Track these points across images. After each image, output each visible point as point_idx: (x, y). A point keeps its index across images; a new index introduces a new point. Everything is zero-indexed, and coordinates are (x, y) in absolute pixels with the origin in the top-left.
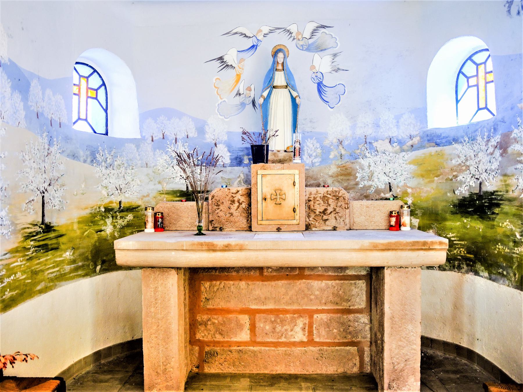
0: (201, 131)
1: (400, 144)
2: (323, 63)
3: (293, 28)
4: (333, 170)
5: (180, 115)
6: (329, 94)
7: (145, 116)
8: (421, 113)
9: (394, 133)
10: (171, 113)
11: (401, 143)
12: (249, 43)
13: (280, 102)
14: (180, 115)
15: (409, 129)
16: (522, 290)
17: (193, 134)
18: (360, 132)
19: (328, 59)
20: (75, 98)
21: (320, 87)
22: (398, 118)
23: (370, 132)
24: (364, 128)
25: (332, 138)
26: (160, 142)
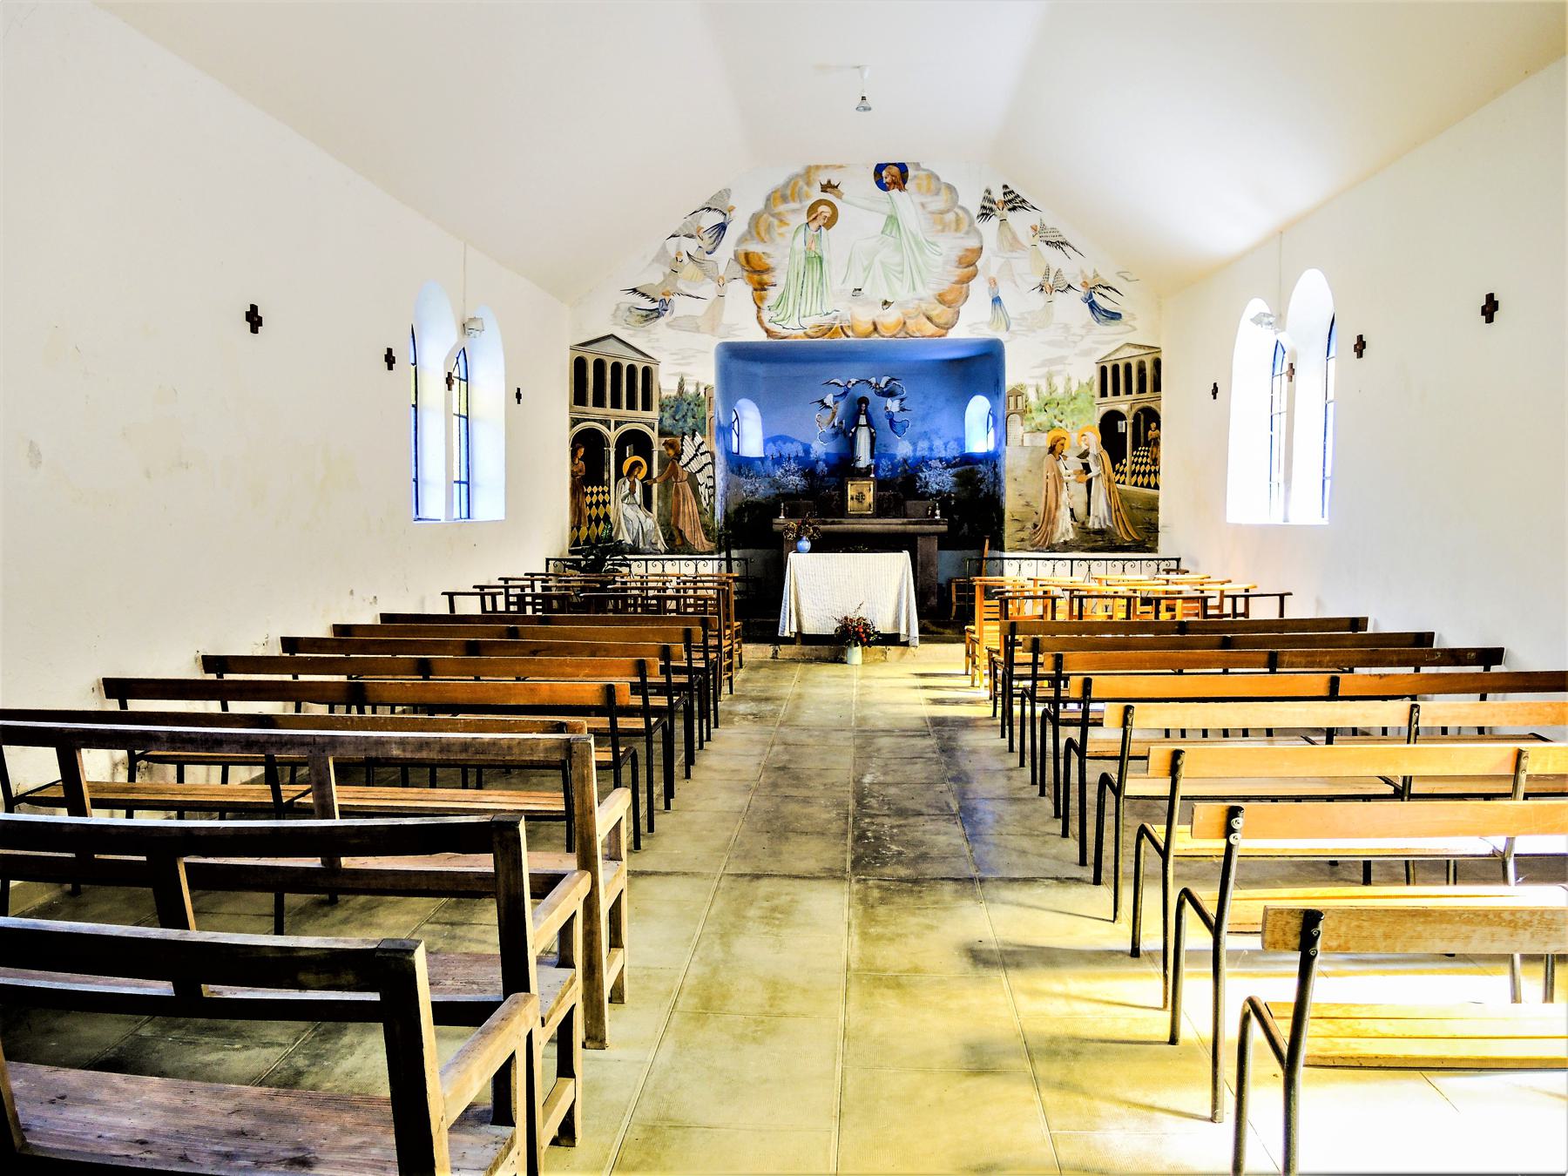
0: (807, 450)
1: (949, 464)
2: (893, 405)
3: (873, 380)
4: (949, 656)
5: (792, 441)
6: (898, 428)
7: (767, 441)
8: (961, 442)
9: (943, 454)
10: (785, 439)
11: (948, 461)
12: (842, 390)
13: (863, 437)
14: (792, 441)
15: (952, 452)
16: (1564, 880)
17: (801, 454)
18: (919, 454)
19: (897, 402)
20: (1317, 682)
21: (892, 423)
22: (946, 445)
23: (926, 453)
24: (922, 449)
25: (899, 458)
26: (778, 461)
